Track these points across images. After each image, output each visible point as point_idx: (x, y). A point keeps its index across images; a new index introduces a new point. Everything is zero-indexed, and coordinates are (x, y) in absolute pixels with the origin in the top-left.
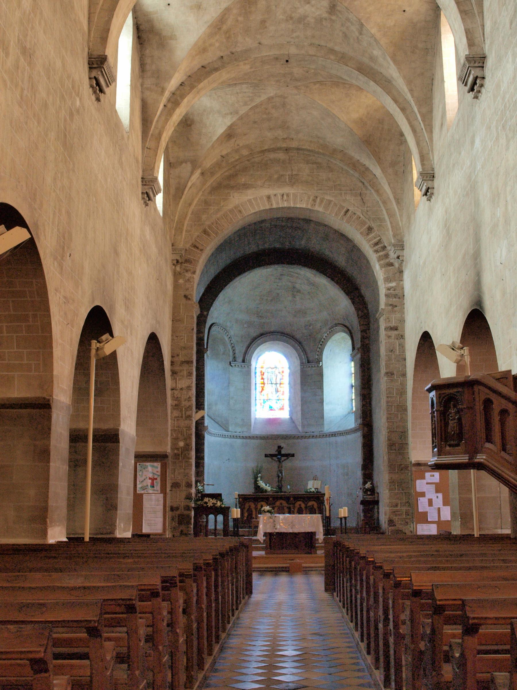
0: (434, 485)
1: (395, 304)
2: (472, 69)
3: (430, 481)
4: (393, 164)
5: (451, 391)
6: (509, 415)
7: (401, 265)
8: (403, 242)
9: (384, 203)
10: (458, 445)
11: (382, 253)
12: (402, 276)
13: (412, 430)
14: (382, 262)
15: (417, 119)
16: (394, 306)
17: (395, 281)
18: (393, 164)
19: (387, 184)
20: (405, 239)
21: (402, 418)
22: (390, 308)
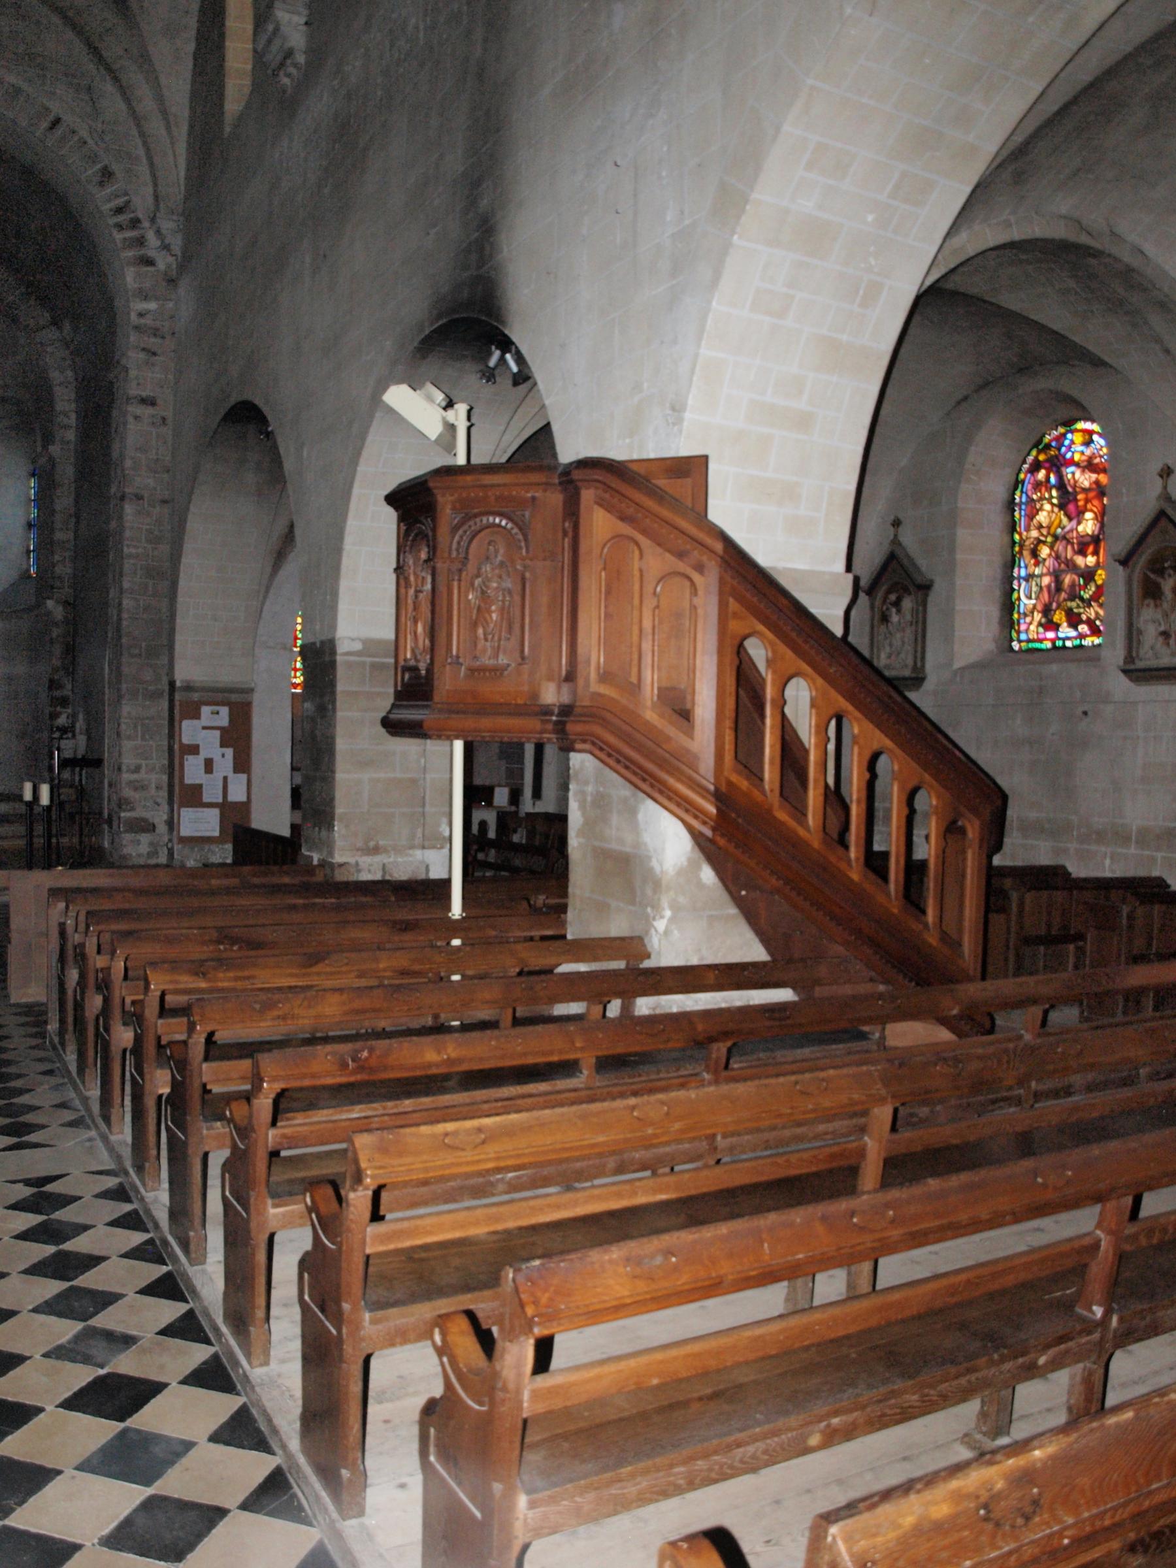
17: (157, 299)
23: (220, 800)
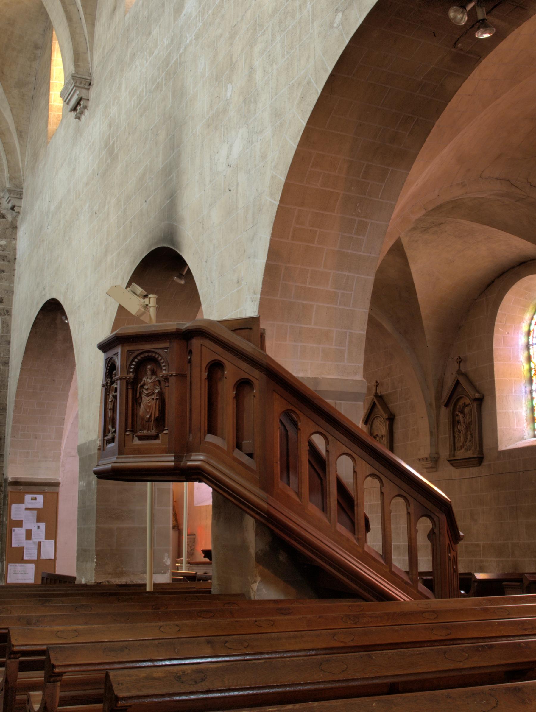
2: (11, 198)
3: (30, 506)
4: (21, 84)
5: (148, 347)
6: (253, 388)
7: (15, 218)
8: (22, 189)
10: (156, 437)
12: (16, 234)
13: (12, 437)
18: (21, 84)
19: (8, 109)
20: (25, 185)
23: (36, 558)
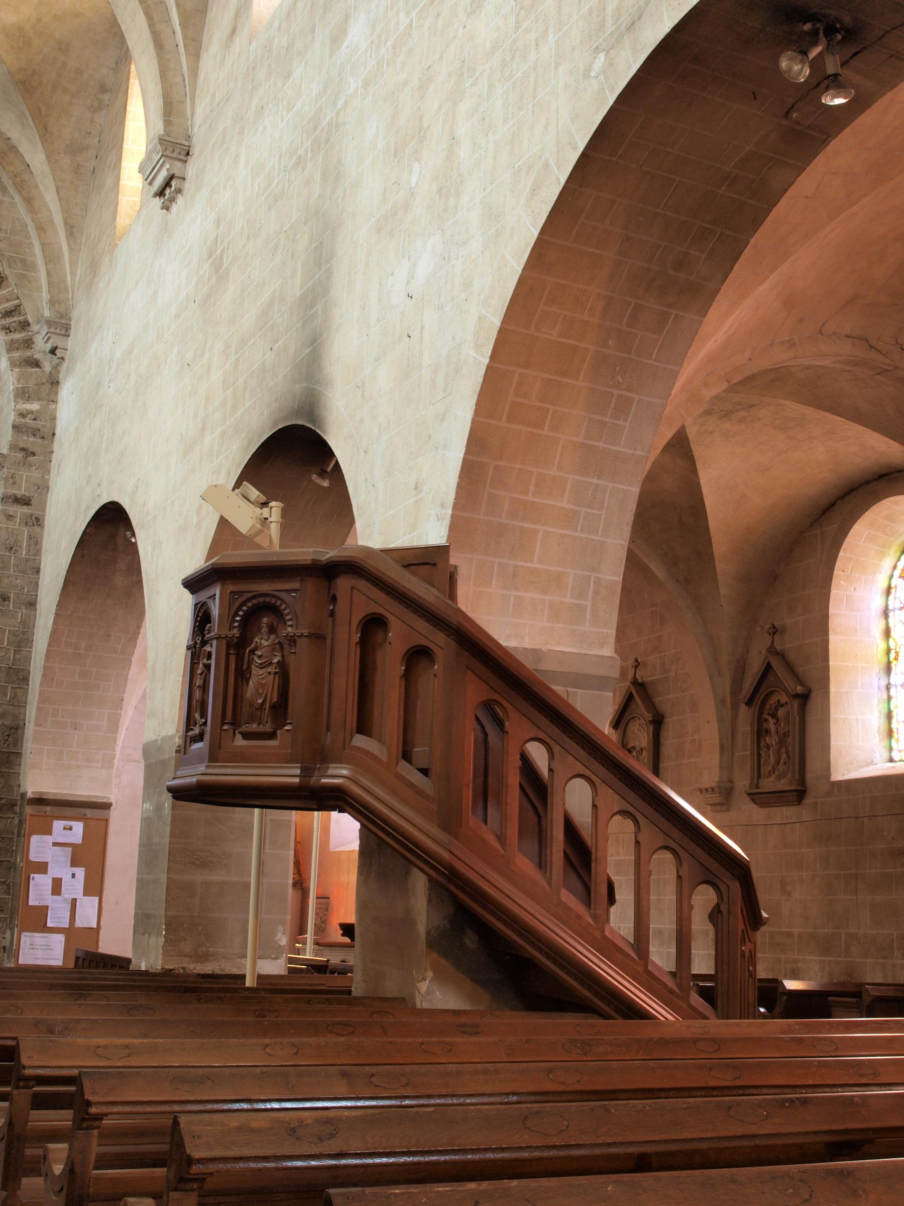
0: (69, 850)
1: (31, 449)
4: (75, 149)
5: (265, 587)
7: (56, 368)
8: (70, 320)
9: (40, 229)
10: (271, 736)
11: (17, 336)
12: (57, 393)
13: (36, 725)
14: (16, 354)
15: (168, 21)
16: (28, 453)
18: (75, 149)
20: (74, 315)
21: (15, 697)
22: (20, 455)
